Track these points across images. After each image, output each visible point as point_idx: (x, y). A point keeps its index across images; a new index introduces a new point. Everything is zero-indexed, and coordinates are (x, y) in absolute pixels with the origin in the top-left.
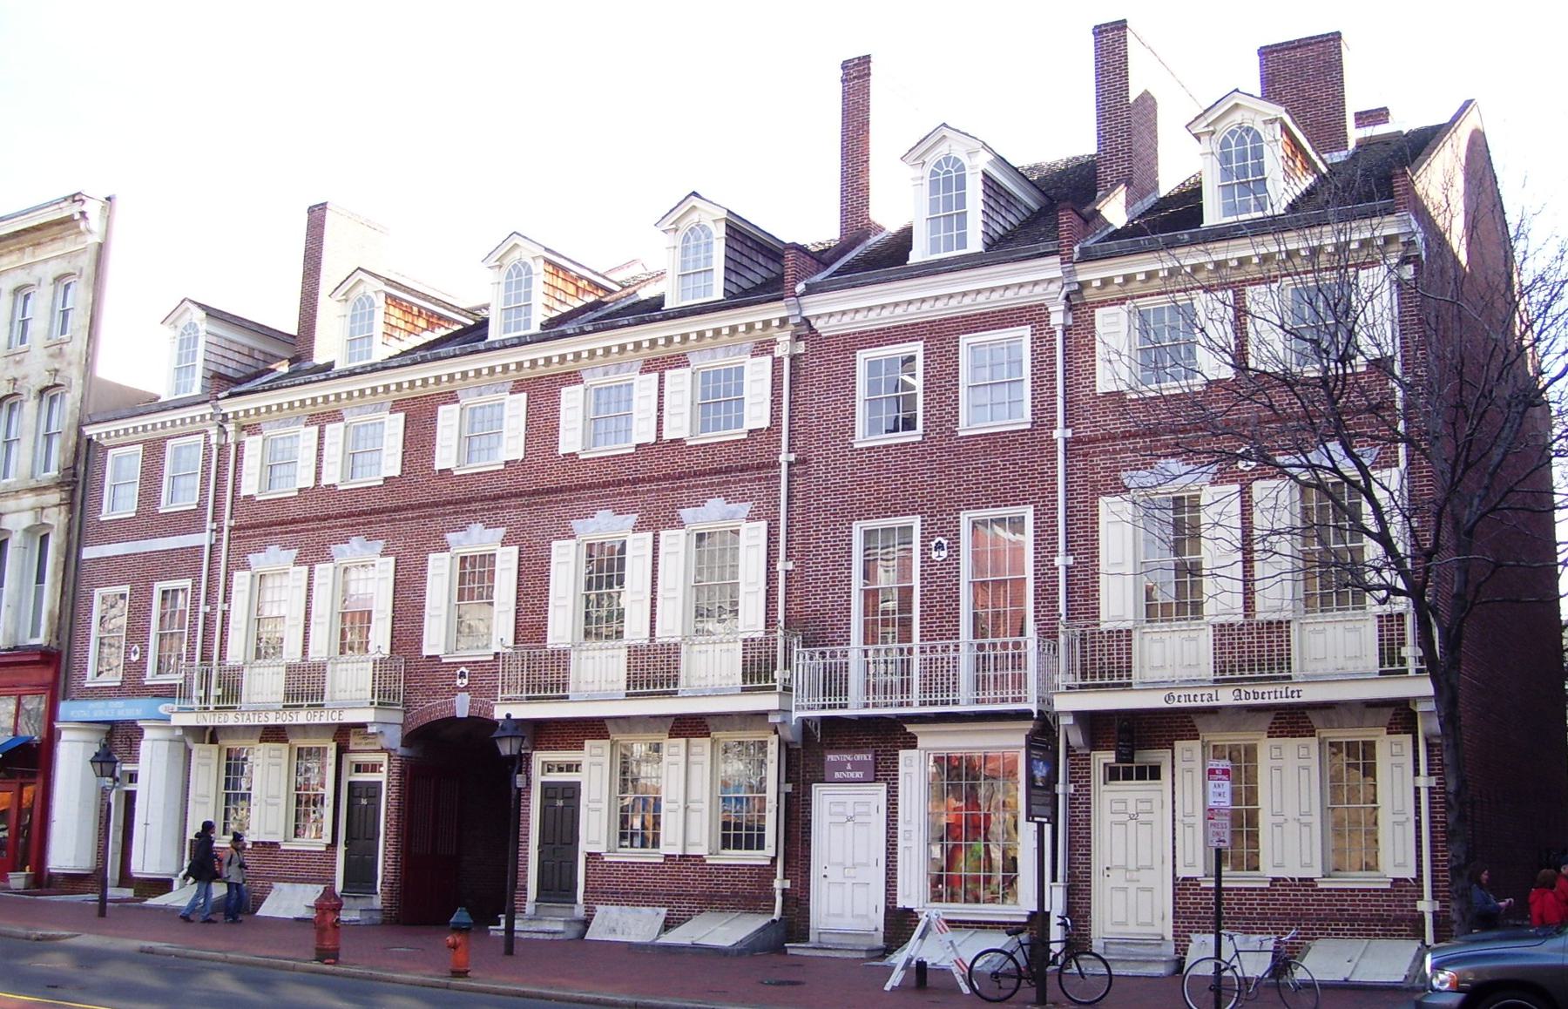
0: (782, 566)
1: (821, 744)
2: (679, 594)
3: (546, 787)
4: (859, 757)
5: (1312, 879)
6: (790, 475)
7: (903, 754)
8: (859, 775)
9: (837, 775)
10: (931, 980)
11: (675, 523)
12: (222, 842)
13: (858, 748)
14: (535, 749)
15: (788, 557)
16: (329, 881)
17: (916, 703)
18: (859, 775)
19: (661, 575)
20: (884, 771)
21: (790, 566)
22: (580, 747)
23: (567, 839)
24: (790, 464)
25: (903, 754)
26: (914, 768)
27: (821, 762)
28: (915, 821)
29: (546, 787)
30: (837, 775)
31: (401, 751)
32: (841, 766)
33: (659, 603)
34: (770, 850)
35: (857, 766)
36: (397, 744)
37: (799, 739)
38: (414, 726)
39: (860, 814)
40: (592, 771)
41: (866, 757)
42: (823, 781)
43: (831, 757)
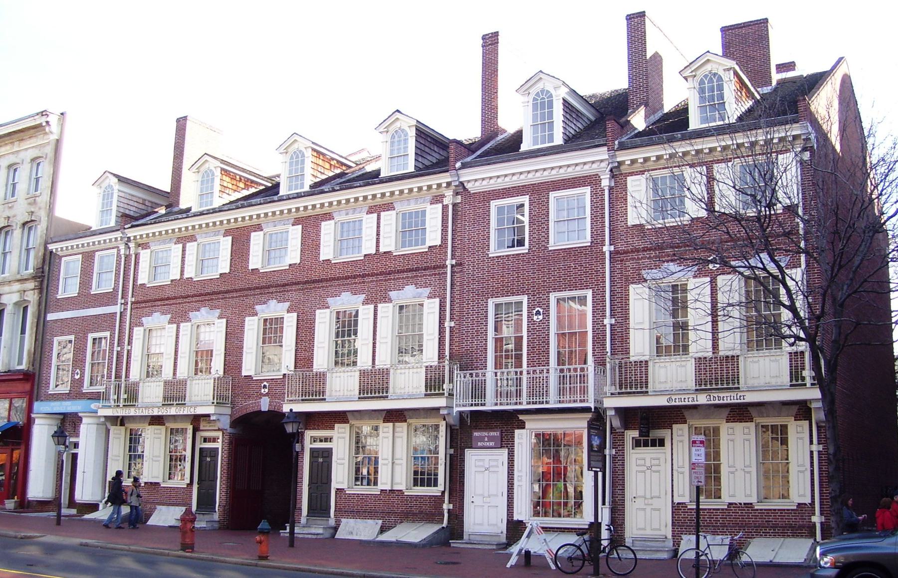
0: (448, 324)
1: (470, 426)
2: (389, 340)
3: (313, 451)
4: (492, 434)
5: (751, 504)
6: (452, 272)
7: (517, 432)
8: (492, 444)
9: (480, 444)
10: (533, 561)
11: (387, 299)
12: (127, 482)
13: (491, 429)
14: (306, 429)
15: (451, 319)
16: (188, 505)
17: (525, 403)
18: (492, 444)
19: (379, 330)
20: (506, 442)
21: (453, 324)
22: (332, 428)
23: (324, 481)
24: (452, 266)
25: (517, 432)
26: (523, 440)
27: (470, 436)
28: (524, 470)
29: (313, 451)
30: (480, 444)
31: (229, 430)
32: (482, 439)
33: (377, 345)
35: (491, 439)
36: (227, 426)
37: (458, 423)
38: (237, 416)
39: (493, 466)
40: (339, 441)
41: (496, 434)
42: (471, 447)
43: (476, 434)
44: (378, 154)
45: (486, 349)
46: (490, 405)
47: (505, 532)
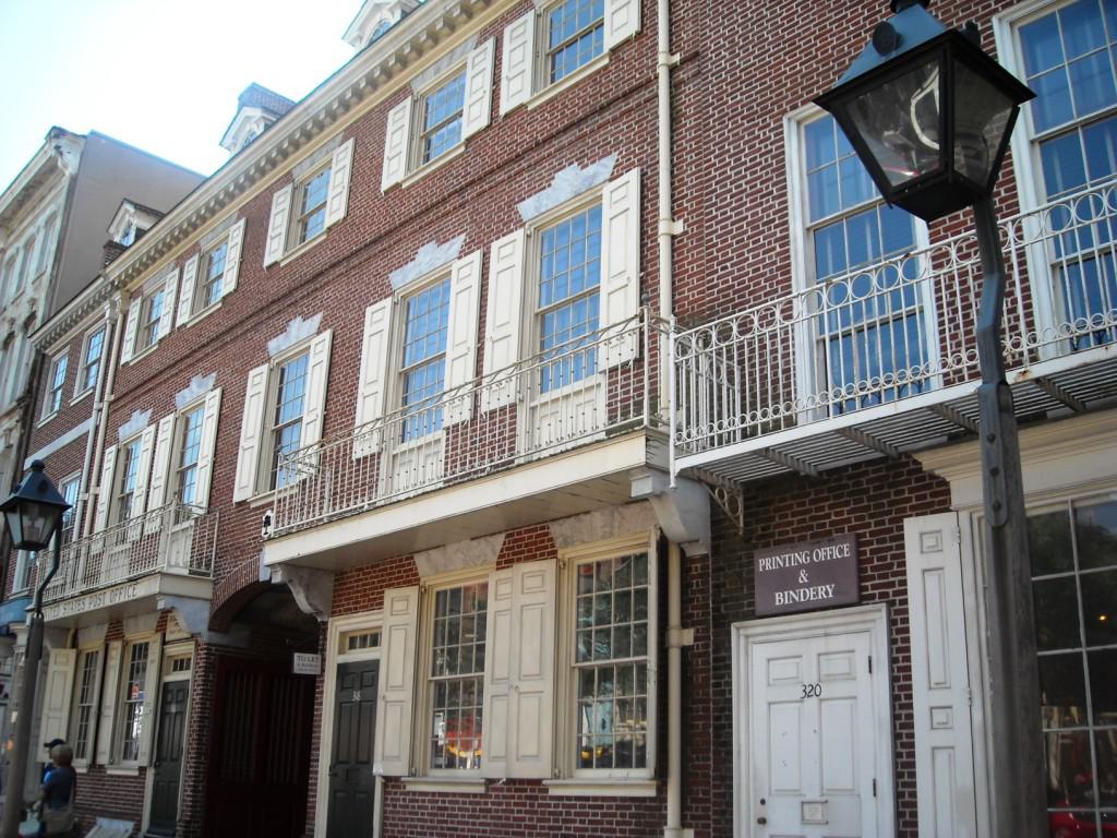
0: (666, 227)
1: (747, 539)
2: (514, 329)
3: (343, 669)
4: (825, 553)
5: (538, 782)
6: (674, 86)
7: (913, 527)
8: (825, 592)
9: (781, 599)
10: (835, 341)
11: (511, 222)
12: (80, 766)
13: (823, 537)
14: (333, 614)
15: (675, 215)
16: (135, 817)
17: (936, 382)
18: (825, 592)
19: (474, 301)
20: (877, 580)
21: (679, 227)
22: (377, 603)
23: (363, 757)
24: (672, 70)
25: (913, 527)
26: (942, 561)
27: (747, 578)
28: (959, 679)
29: (343, 669)
30: (781, 599)
31: (205, 636)
32: (786, 579)
33: (472, 343)
34: (143, 761)
35: (820, 573)
36: (203, 628)
37: (705, 534)
38: (223, 599)
39: (832, 678)
40: (394, 635)
41: (838, 551)
42: (752, 616)
43: (766, 563)
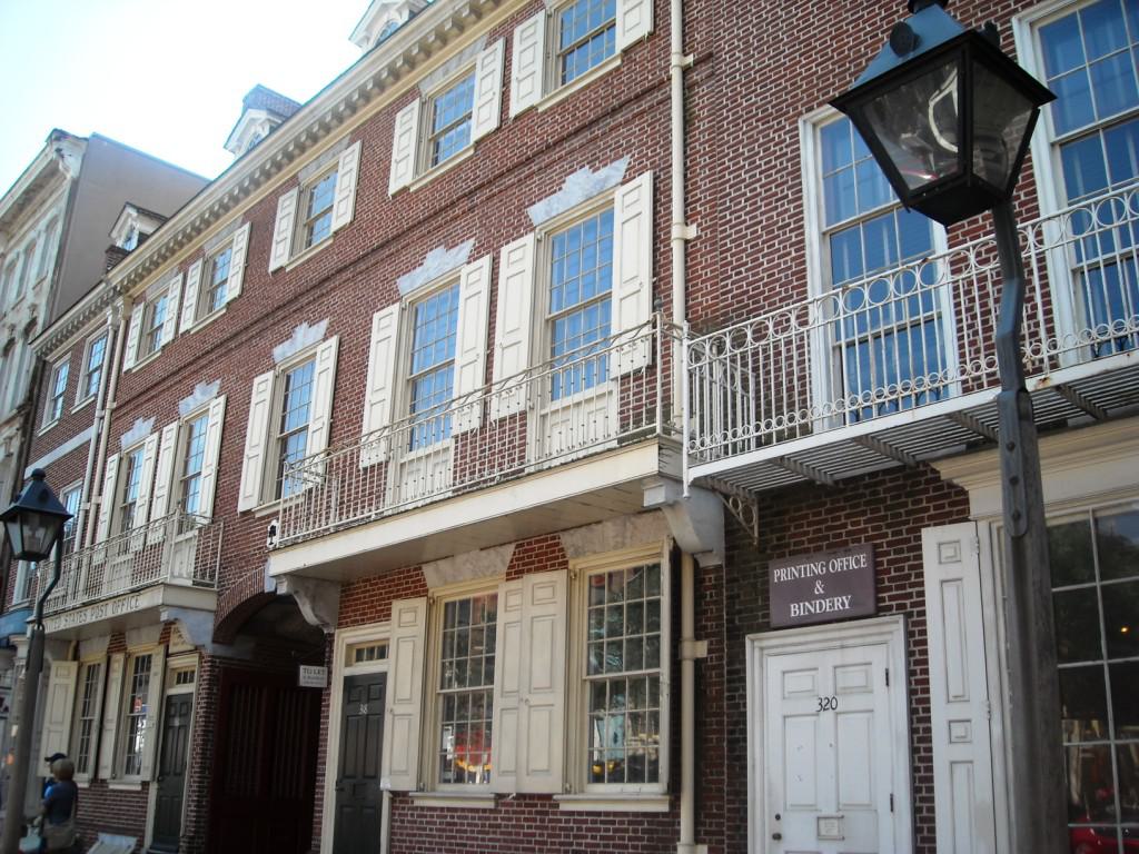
0: (679, 231)
1: (762, 550)
2: (524, 336)
3: (350, 682)
4: (842, 564)
6: (687, 88)
7: (931, 537)
8: (841, 603)
9: (797, 610)
10: (851, 348)
11: (521, 226)
12: (82, 780)
13: (839, 547)
14: (340, 625)
15: (688, 219)
16: (138, 832)
17: (955, 389)
18: (841, 603)
19: (484, 307)
20: (894, 591)
21: (692, 232)
22: (385, 615)
23: (370, 772)
24: (686, 71)
25: (931, 537)
26: (960, 572)
27: (762, 589)
28: (978, 692)
29: (350, 682)
30: (797, 610)
31: (210, 649)
32: (802, 590)
33: (482, 350)
34: (146, 775)
35: (836, 584)
36: (207, 640)
37: (719, 545)
38: (227, 610)
39: (848, 691)
40: (402, 647)
41: (854, 562)
42: (767, 627)
43: (781, 574)
44: (710, 548)
45: (796, 173)
46: (829, 428)
47: (300, 606)
